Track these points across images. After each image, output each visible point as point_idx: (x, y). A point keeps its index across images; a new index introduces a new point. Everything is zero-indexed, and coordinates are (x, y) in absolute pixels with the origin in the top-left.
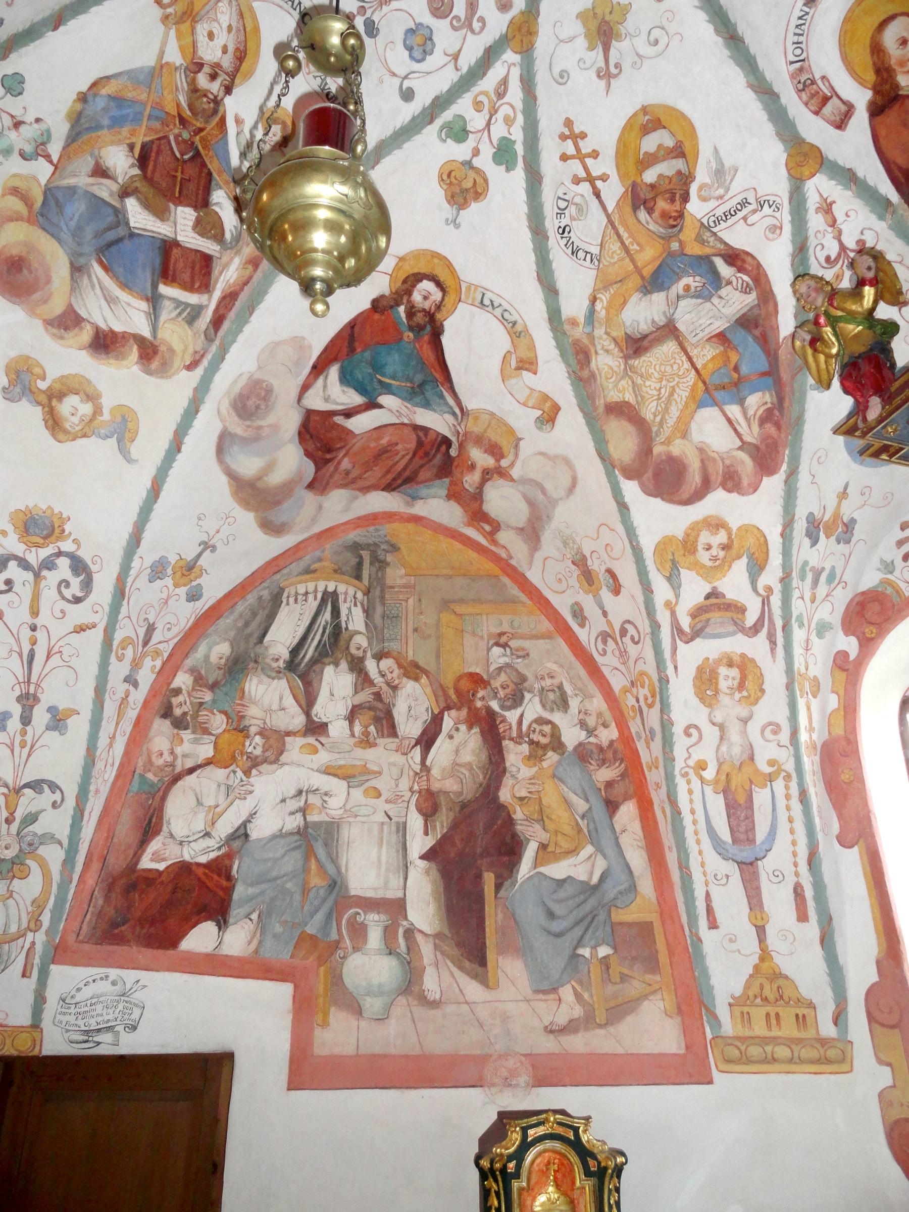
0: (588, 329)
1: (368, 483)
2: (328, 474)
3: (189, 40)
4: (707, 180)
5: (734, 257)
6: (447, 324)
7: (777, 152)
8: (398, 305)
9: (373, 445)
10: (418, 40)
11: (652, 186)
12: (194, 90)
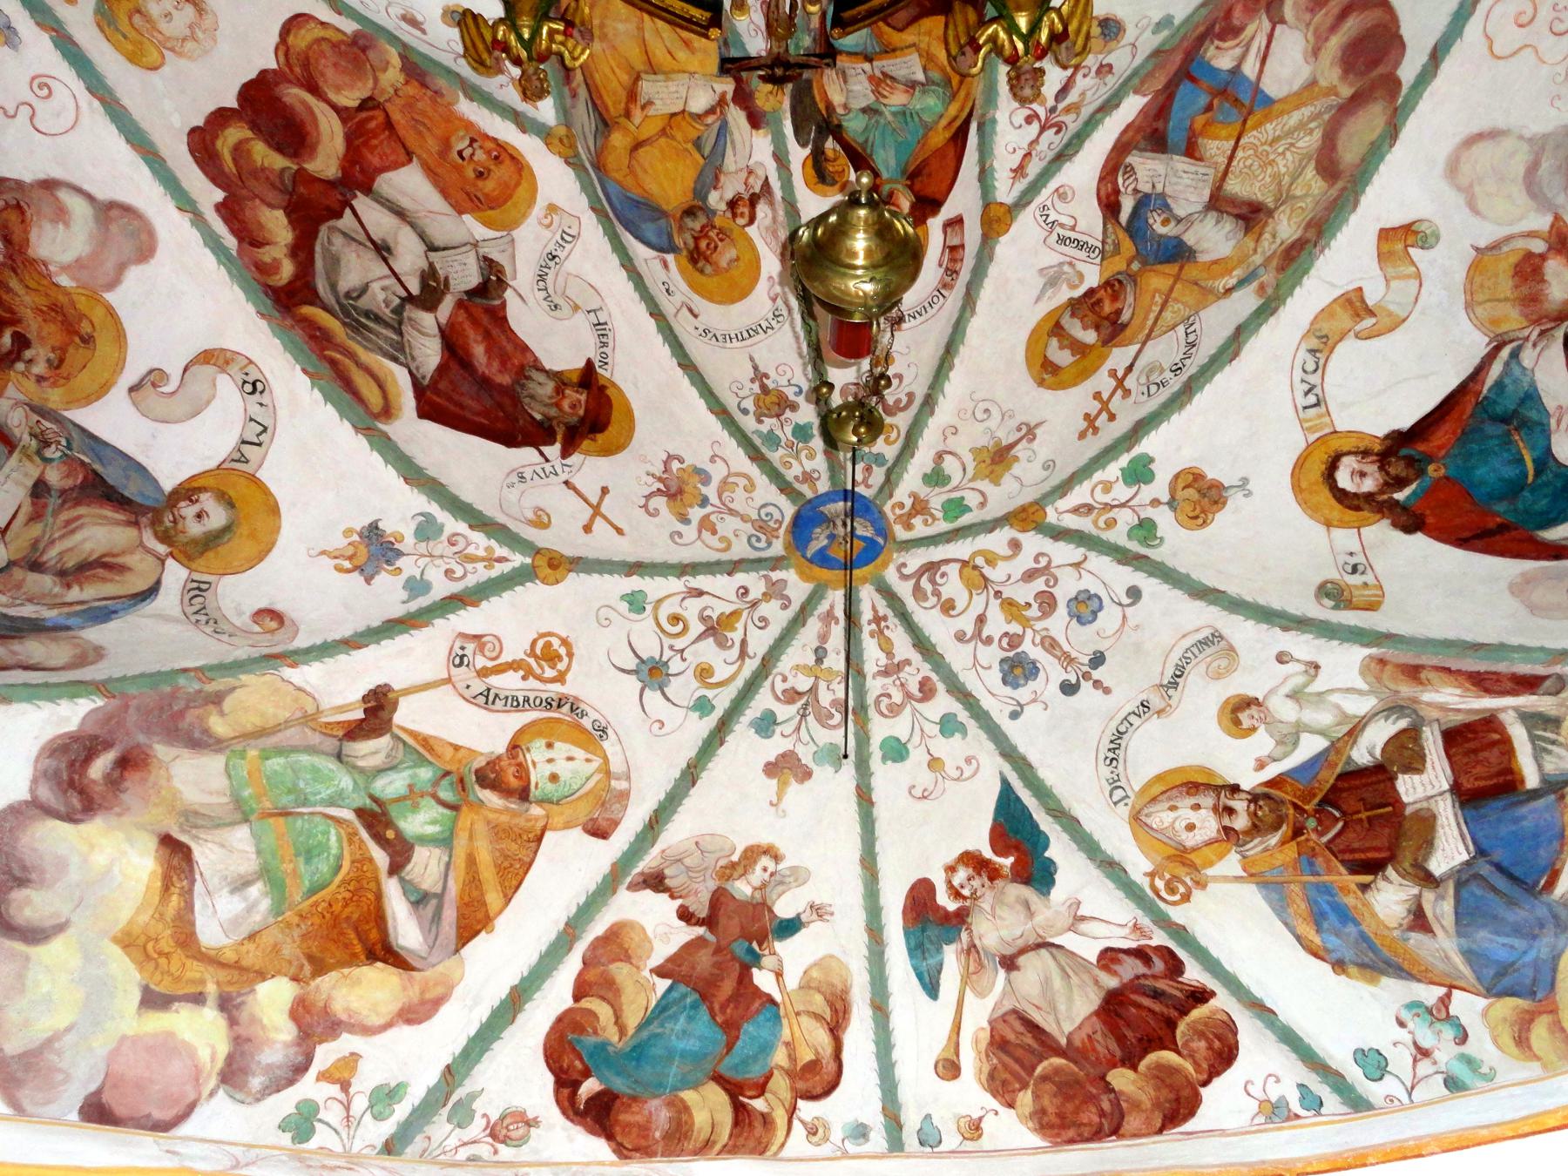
0: (1262, 271)
3: (1206, 851)
4: (1064, 286)
5: (1110, 207)
6: (1381, 432)
7: (1005, 247)
8: (1397, 502)
10: (1083, 609)
11: (1097, 328)
12: (1256, 829)
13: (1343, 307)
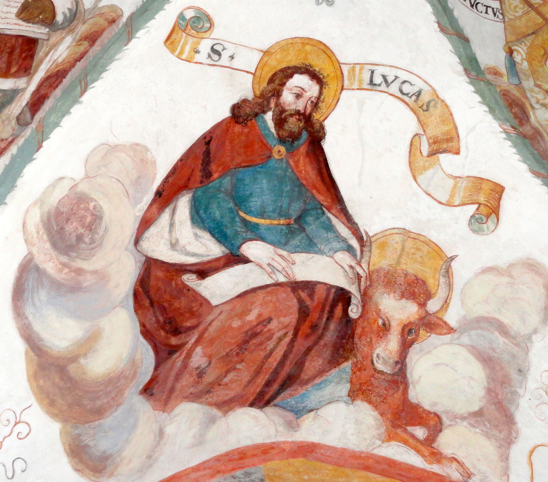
1: (231, 394)
2: (173, 373)
6: (328, 124)
8: (264, 112)
9: (236, 324)
13: (448, 133)
